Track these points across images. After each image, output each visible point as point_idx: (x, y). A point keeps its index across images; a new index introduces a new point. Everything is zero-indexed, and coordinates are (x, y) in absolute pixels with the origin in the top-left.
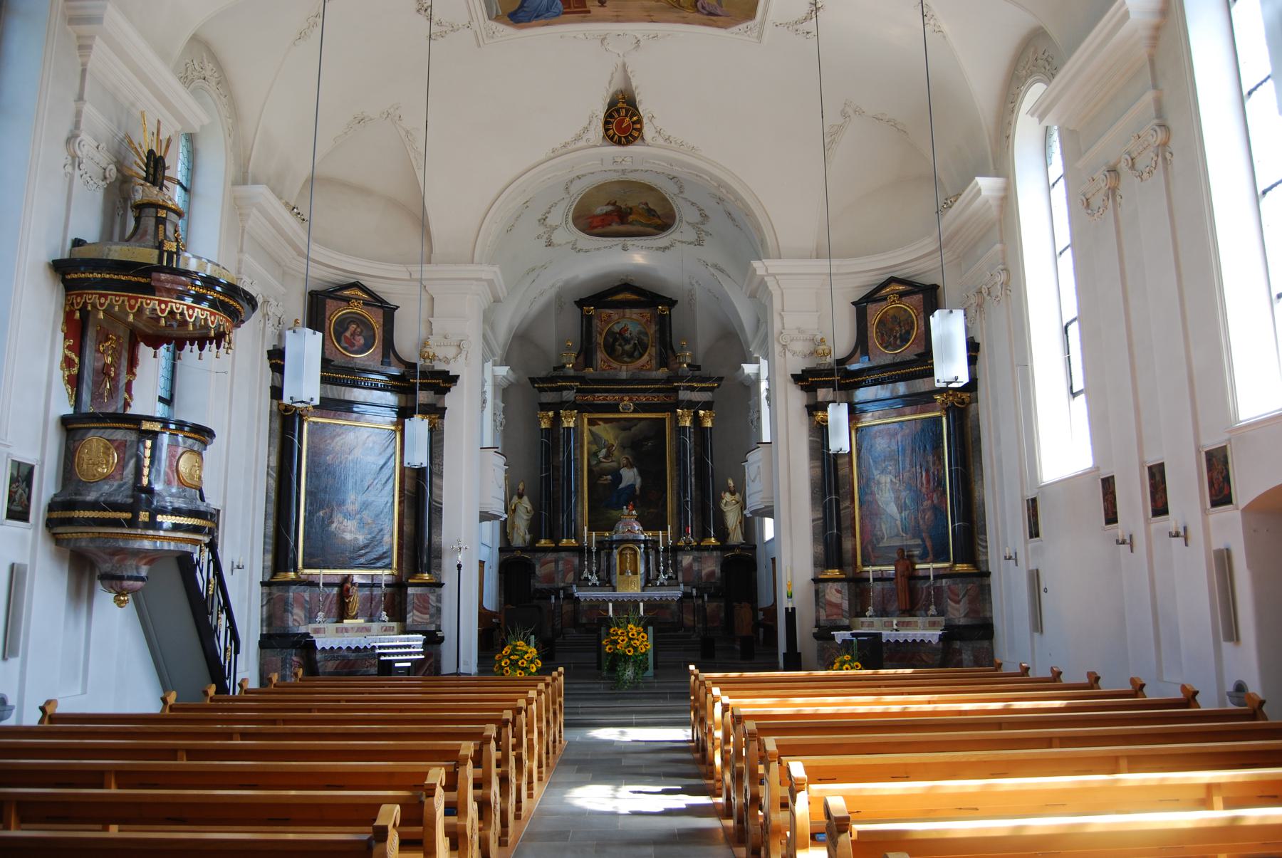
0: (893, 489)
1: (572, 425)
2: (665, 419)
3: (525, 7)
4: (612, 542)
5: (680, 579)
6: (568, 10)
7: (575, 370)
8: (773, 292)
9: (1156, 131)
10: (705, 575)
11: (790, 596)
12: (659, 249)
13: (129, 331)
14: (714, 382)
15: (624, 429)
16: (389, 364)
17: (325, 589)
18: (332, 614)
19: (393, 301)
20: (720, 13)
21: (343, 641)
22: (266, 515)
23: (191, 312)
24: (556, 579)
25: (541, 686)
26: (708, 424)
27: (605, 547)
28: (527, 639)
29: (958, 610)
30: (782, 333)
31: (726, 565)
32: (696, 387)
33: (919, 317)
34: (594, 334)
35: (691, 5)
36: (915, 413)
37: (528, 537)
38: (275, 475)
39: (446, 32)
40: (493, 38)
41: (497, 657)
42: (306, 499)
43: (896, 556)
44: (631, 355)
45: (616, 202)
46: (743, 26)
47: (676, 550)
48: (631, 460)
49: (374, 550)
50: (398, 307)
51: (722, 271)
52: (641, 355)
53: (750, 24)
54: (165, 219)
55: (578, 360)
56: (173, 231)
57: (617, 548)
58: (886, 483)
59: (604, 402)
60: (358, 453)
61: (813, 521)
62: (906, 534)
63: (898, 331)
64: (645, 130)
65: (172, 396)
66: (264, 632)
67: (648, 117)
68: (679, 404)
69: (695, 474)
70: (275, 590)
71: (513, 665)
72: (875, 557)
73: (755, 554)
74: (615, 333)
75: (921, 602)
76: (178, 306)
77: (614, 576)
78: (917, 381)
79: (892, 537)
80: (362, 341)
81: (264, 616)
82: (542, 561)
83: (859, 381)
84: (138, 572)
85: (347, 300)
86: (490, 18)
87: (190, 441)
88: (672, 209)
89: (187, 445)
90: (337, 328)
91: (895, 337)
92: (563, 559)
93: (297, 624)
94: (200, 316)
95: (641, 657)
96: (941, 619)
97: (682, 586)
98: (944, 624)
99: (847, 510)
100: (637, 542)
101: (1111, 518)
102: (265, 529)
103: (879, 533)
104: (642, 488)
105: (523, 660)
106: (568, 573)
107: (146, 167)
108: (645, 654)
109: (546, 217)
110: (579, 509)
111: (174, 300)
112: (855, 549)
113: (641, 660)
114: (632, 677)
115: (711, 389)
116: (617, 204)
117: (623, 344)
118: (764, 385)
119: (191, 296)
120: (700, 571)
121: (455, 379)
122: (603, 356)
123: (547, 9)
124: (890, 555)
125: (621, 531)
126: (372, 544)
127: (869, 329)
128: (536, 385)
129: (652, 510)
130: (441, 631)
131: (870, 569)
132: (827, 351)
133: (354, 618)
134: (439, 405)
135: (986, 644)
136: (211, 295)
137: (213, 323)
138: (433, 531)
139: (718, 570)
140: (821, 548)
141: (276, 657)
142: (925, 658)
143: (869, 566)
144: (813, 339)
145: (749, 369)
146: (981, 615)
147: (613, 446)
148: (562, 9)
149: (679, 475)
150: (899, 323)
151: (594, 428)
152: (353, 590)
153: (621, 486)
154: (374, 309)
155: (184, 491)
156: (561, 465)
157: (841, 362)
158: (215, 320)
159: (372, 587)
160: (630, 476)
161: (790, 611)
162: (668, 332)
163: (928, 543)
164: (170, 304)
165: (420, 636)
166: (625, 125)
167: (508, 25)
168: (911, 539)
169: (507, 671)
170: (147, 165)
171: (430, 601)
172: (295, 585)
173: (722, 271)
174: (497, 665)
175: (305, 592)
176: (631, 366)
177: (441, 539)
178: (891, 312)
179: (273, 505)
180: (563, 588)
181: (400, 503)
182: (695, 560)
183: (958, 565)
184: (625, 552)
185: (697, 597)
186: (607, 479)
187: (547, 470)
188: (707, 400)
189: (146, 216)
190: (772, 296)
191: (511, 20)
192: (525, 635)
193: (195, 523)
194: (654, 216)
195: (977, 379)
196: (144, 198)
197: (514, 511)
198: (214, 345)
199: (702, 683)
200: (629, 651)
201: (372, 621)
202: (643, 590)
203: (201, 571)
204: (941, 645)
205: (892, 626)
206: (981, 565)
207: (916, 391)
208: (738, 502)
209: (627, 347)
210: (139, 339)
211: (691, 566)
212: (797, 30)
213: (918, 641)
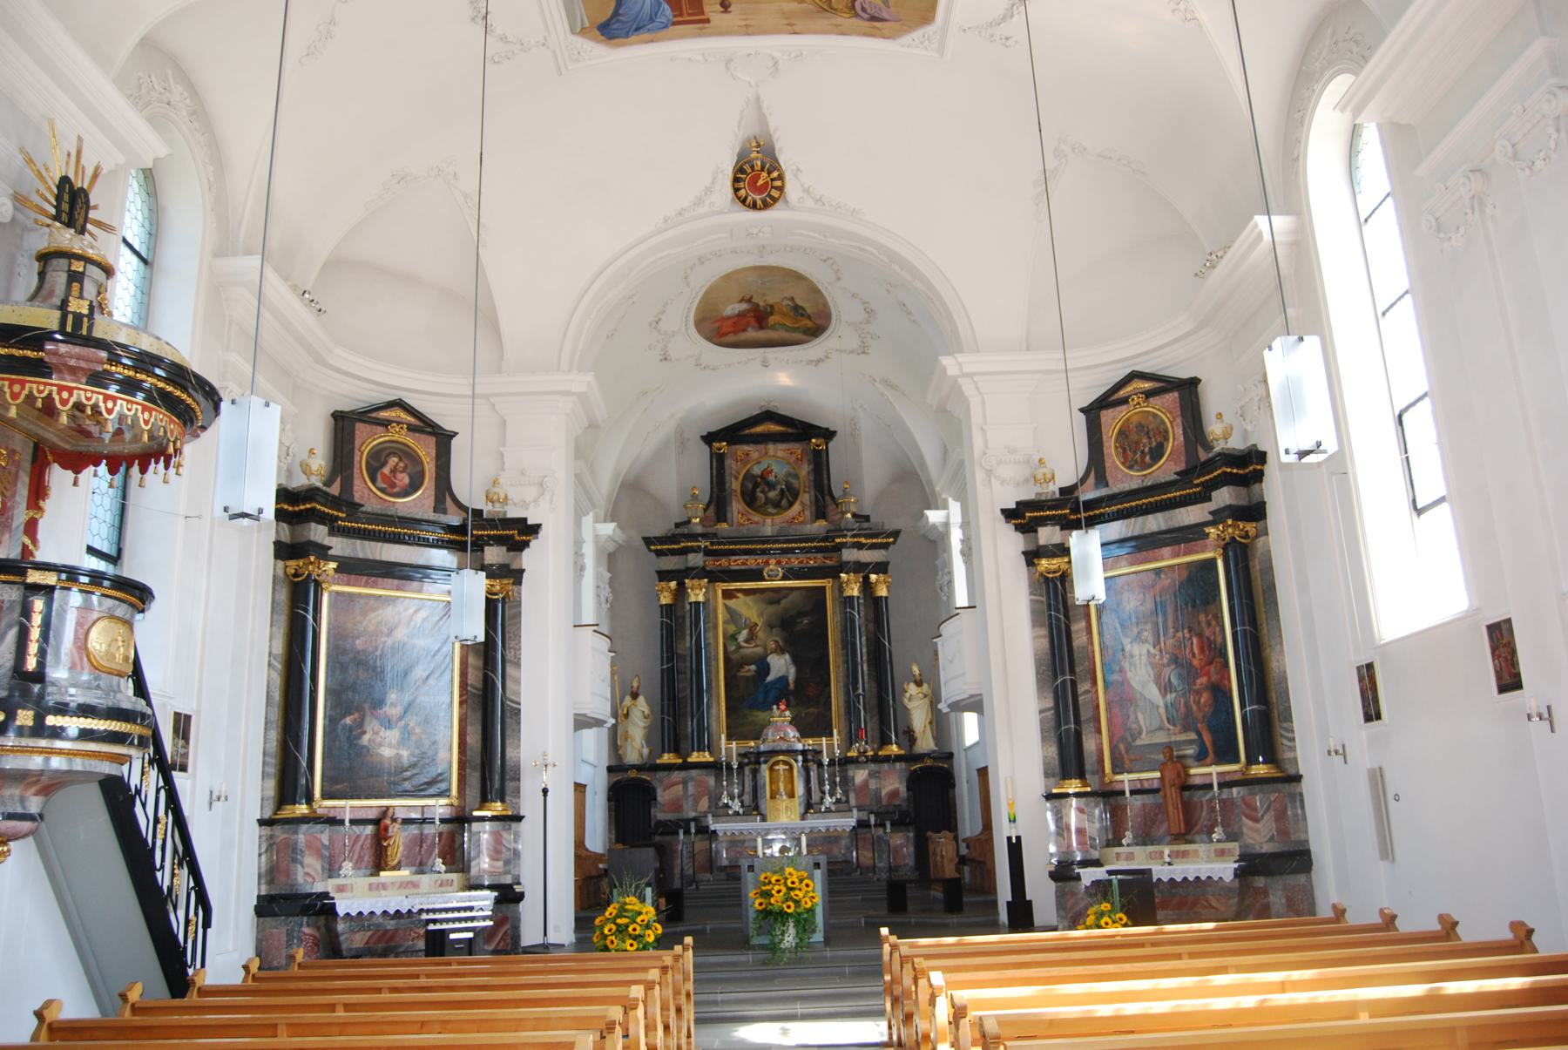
0: (1151, 664)
1: (701, 598)
2: (824, 587)
3: (620, 15)
4: (759, 754)
5: (853, 801)
6: (680, 19)
7: (704, 526)
8: (970, 399)
9: (1469, 178)
10: (886, 794)
11: (1013, 820)
12: (810, 362)
13: (32, 445)
14: (888, 536)
15: (771, 602)
16: (445, 512)
17: (354, 827)
18: (364, 864)
19: (448, 425)
20: (887, 17)
21: (377, 903)
22: (266, 724)
23: (110, 405)
24: (685, 807)
25: (654, 974)
26: (882, 591)
27: (753, 760)
28: (641, 893)
29: (1257, 831)
30: (985, 454)
31: (913, 781)
32: (866, 544)
33: (1175, 423)
34: (727, 478)
35: (846, 7)
36: (1177, 555)
37: (646, 751)
38: (280, 667)
39: (513, 52)
40: (577, 61)
41: (597, 921)
42: (326, 700)
43: (1161, 757)
44: (777, 505)
45: (752, 297)
46: (918, 34)
47: (846, 762)
48: (781, 643)
49: (425, 771)
50: (456, 434)
51: (893, 387)
52: (791, 504)
53: (928, 30)
54: (83, 274)
55: (708, 512)
56: (94, 292)
57: (765, 762)
58: (1140, 655)
59: (743, 567)
60: (400, 634)
61: (1041, 712)
62: (1174, 725)
63: (1146, 445)
64: (788, 188)
65: (120, 551)
66: (263, 893)
67: (793, 171)
68: (843, 567)
69: (868, 661)
70: (278, 830)
71: (621, 932)
72: (1131, 760)
73: (951, 765)
74: (754, 477)
75: (1200, 823)
76: (89, 395)
77: (763, 800)
78: (1177, 510)
79: (1152, 732)
80: (407, 480)
81: (263, 870)
82: (665, 783)
83: (1095, 515)
84: (24, 808)
85: (386, 424)
86: (573, 32)
87: (109, 602)
88: (826, 304)
89: (104, 608)
90: (371, 461)
91: (1143, 452)
92: (692, 779)
93: (310, 880)
94: (126, 411)
95: (805, 916)
96: (1234, 846)
97: (855, 811)
98: (1238, 853)
99: (1087, 696)
100: (791, 752)
101: (1509, 680)
102: (265, 743)
103: (1134, 726)
104: (797, 681)
105: (635, 925)
106: (700, 799)
107: (56, 201)
108: (811, 911)
109: (660, 319)
110: (714, 711)
111: (82, 386)
112: (1100, 751)
113: (806, 920)
114: (793, 945)
115: (885, 546)
116: (753, 300)
117: (766, 489)
118: (956, 536)
119: (117, 382)
120: (878, 791)
121: (534, 530)
122: (740, 508)
123: (651, 18)
124: (1152, 756)
125: (771, 740)
126: (421, 763)
127: (1106, 444)
128: (653, 547)
129: (811, 710)
130: (519, 883)
131: (1126, 777)
132: (1049, 476)
133: (394, 868)
134: (514, 566)
135: (1302, 878)
136: (149, 382)
137: (146, 423)
138: (508, 742)
139: (903, 789)
140: (1053, 751)
141: (279, 928)
142: (1214, 903)
143: (1122, 773)
144: (1028, 462)
145: (934, 516)
146: (1293, 838)
147: (757, 625)
148: (671, 17)
149: (847, 662)
150: (1148, 433)
151: (731, 603)
152: (394, 829)
153: (770, 678)
154: (423, 436)
155: (96, 679)
156: (689, 653)
157: (1067, 491)
158: (156, 420)
159: (421, 823)
160: (781, 665)
161: (1014, 841)
162: (825, 472)
163: (1207, 738)
164: (75, 392)
165: (487, 893)
166: (760, 182)
167: (598, 42)
168: (1180, 733)
169: (612, 942)
170: (59, 198)
171: (504, 842)
172: (308, 823)
173: (893, 387)
174: (598, 933)
175: (322, 832)
176: (778, 519)
177: (519, 753)
178: (1135, 420)
179: (276, 709)
180: (695, 819)
181: (461, 703)
182: (871, 775)
183: (1254, 767)
184: (777, 768)
185: (876, 825)
186: (749, 670)
187: (670, 660)
188: (879, 560)
189: (54, 271)
190: (969, 405)
191: (602, 35)
192: (637, 887)
193: (117, 729)
194: (802, 315)
195: (1265, 503)
196: (52, 245)
197: (627, 716)
198: (162, 464)
199: (904, 960)
200: (789, 907)
201: (423, 872)
202: (803, 817)
203: (144, 805)
204: (1236, 884)
205: (1162, 857)
206: (1287, 766)
207: (1177, 526)
208: (925, 696)
209: (772, 494)
210: (50, 458)
211: (866, 784)
212: (992, 36)
213: (1191, 879)
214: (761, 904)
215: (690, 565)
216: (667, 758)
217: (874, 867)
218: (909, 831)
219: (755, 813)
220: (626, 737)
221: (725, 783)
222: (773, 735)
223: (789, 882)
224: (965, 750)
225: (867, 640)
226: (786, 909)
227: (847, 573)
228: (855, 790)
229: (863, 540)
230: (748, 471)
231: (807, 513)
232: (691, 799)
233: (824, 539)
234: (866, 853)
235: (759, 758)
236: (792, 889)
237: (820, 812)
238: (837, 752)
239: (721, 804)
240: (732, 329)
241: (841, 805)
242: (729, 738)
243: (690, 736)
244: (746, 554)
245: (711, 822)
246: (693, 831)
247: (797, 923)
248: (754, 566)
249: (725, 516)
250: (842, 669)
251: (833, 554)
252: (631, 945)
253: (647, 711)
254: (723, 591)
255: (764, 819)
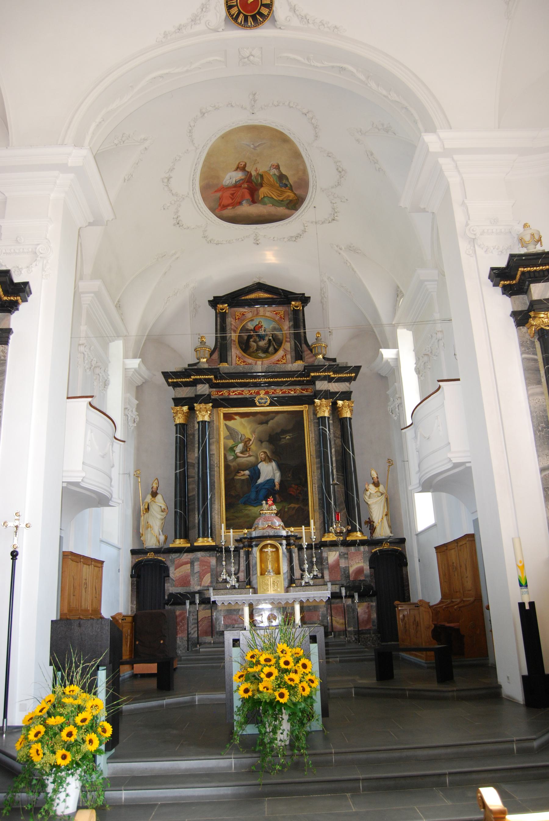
1: (207, 418)
5: (327, 577)
10: (353, 571)
12: (290, 239)
15: (261, 423)
26: (347, 414)
31: (374, 560)
32: (333, 378)
37: (162, 538)
44: (266, 351)
45: (245, 165)
52: (276, 351)
57: (257, 545)
59: (240, 396)
73: (404, 548)
82: (176, 562)
92: (198, 559)
97: (329, 585)
104: (282, 483)
110: (216, 506)
113: (303, 711)
115: (349, 380)
116: (247, 169)
117: (258, 340)
128: (170, 380)
129: (292, 505)
139: (366, 567)
144: (510, 232)
145: (387, 354)
147: (250, 440)
151: (230, 423)
153: (260, 481)
161: (527, 607)
176: (267, 362)
180: (199, 592)
184: (266, 550)
185: (346, 597)
186: (244, 475)
194: (286, 185)
200: (282, 695)
202: (287, 590)
208: (382, 494)
209: (262, 343)
211: (337, 563)
214: (246, 691)
215: (199, 393)
216: (180, 543)
217: (346, 630)
218: (372, 602)
219: (248, 587)
220: (148, 526)
221: (224, 563)
222: (263, 524)
223: (281, 662)
224: (417, 535)
225: (336, 451)
226: (278, 698)
227: (319, 399)
228: (328, 568)
229: (332, 374)
230: (243, 326)
231: (289, 357)
232: (197, 575)
233: (301, 375)
234: (338, 619)
235: (252, 542)
236: (286, 671)
237: (301, 586)
238: (314, 537)
239: (220, 580)
240: (230, 201)
241: (317, 580)
242: (228, 527)
243: (197, 525)
244: (241, 387)
245: (212, 594)
246: (197, 601)
247: (292, 715)
248: (248, 396)
249: (227, 359)
250: (200, 769)
251: (307, 387)
252: (64, 757)
253: (163, 506)
254: (224, 414)
255: (255, 592)
